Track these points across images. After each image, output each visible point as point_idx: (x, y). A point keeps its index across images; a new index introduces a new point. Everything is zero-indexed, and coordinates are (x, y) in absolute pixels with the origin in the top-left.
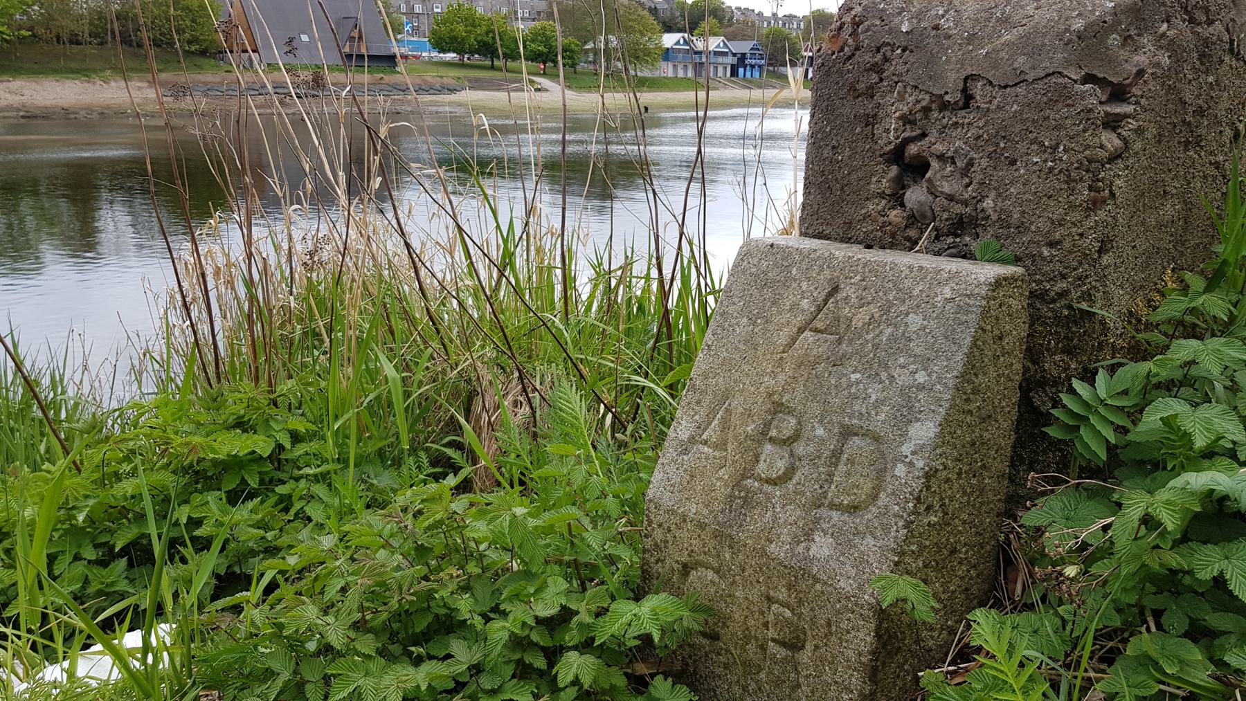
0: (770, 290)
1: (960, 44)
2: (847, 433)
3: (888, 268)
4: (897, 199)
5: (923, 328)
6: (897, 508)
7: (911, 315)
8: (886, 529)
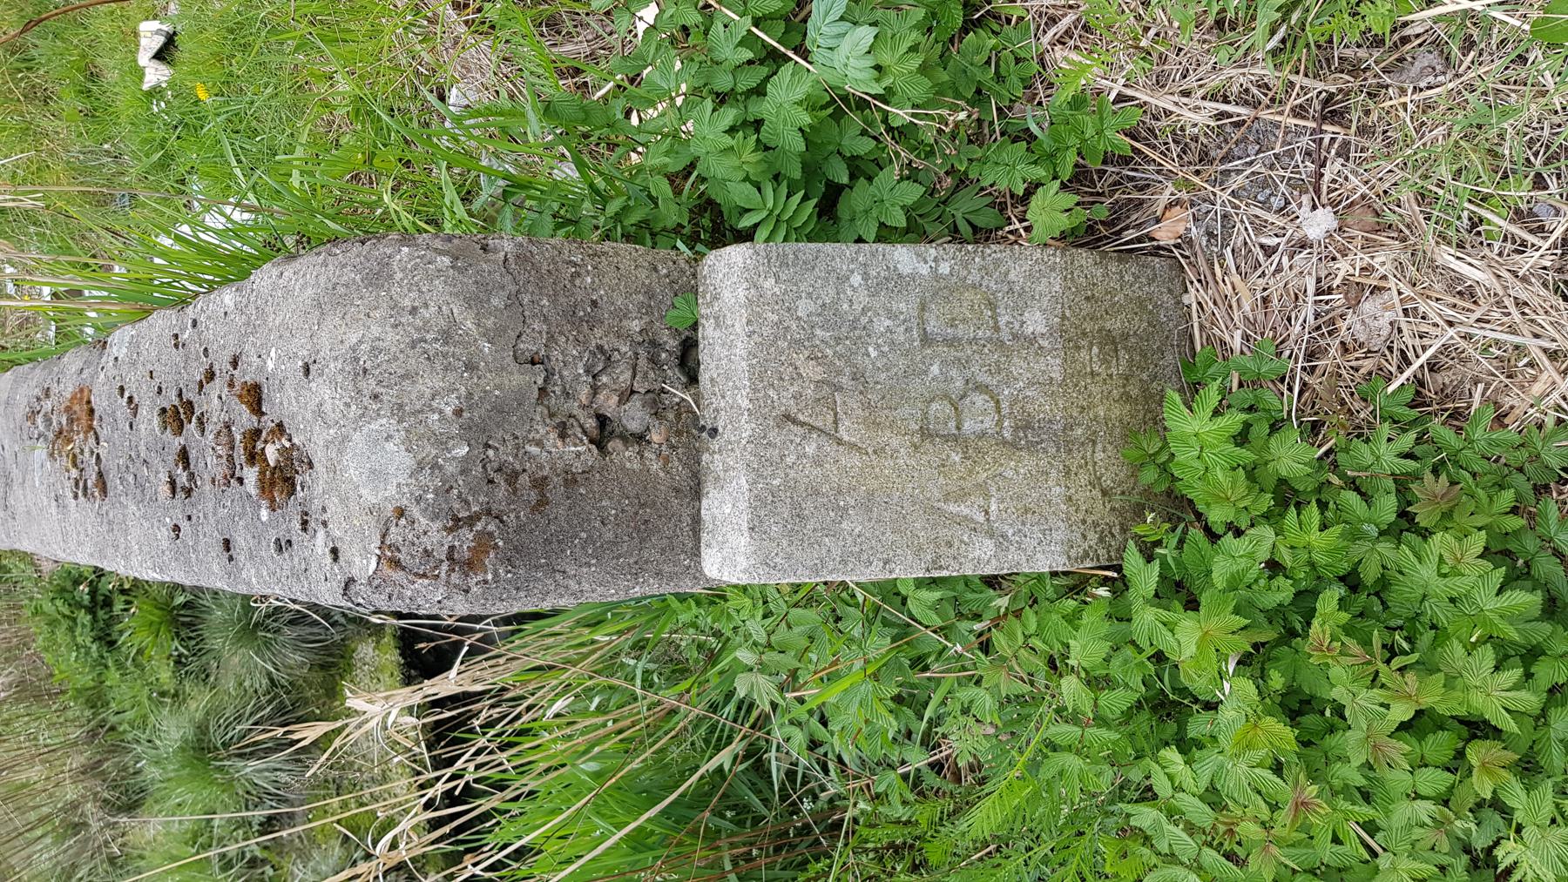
0: (804, 506)
1: (479, 378)
2: (926, 340)
3: (754, 362)
4: (640, 438)
5: (809, 295)
6: (977, 260)
7: (799, 314)
8: (997, 263)
